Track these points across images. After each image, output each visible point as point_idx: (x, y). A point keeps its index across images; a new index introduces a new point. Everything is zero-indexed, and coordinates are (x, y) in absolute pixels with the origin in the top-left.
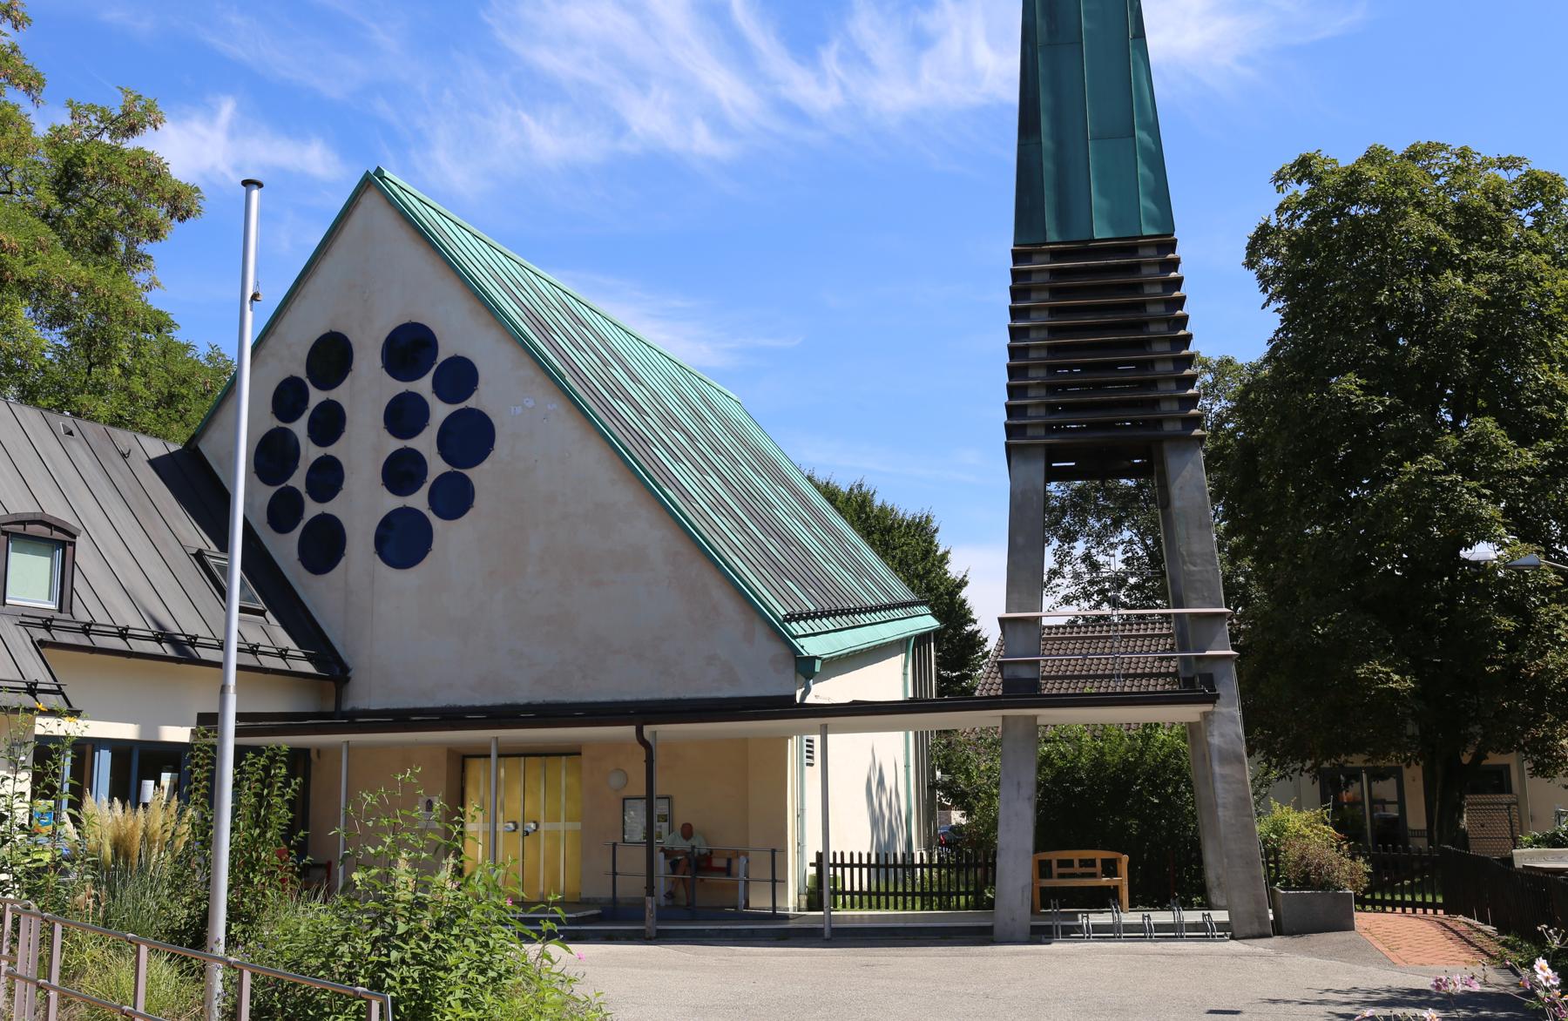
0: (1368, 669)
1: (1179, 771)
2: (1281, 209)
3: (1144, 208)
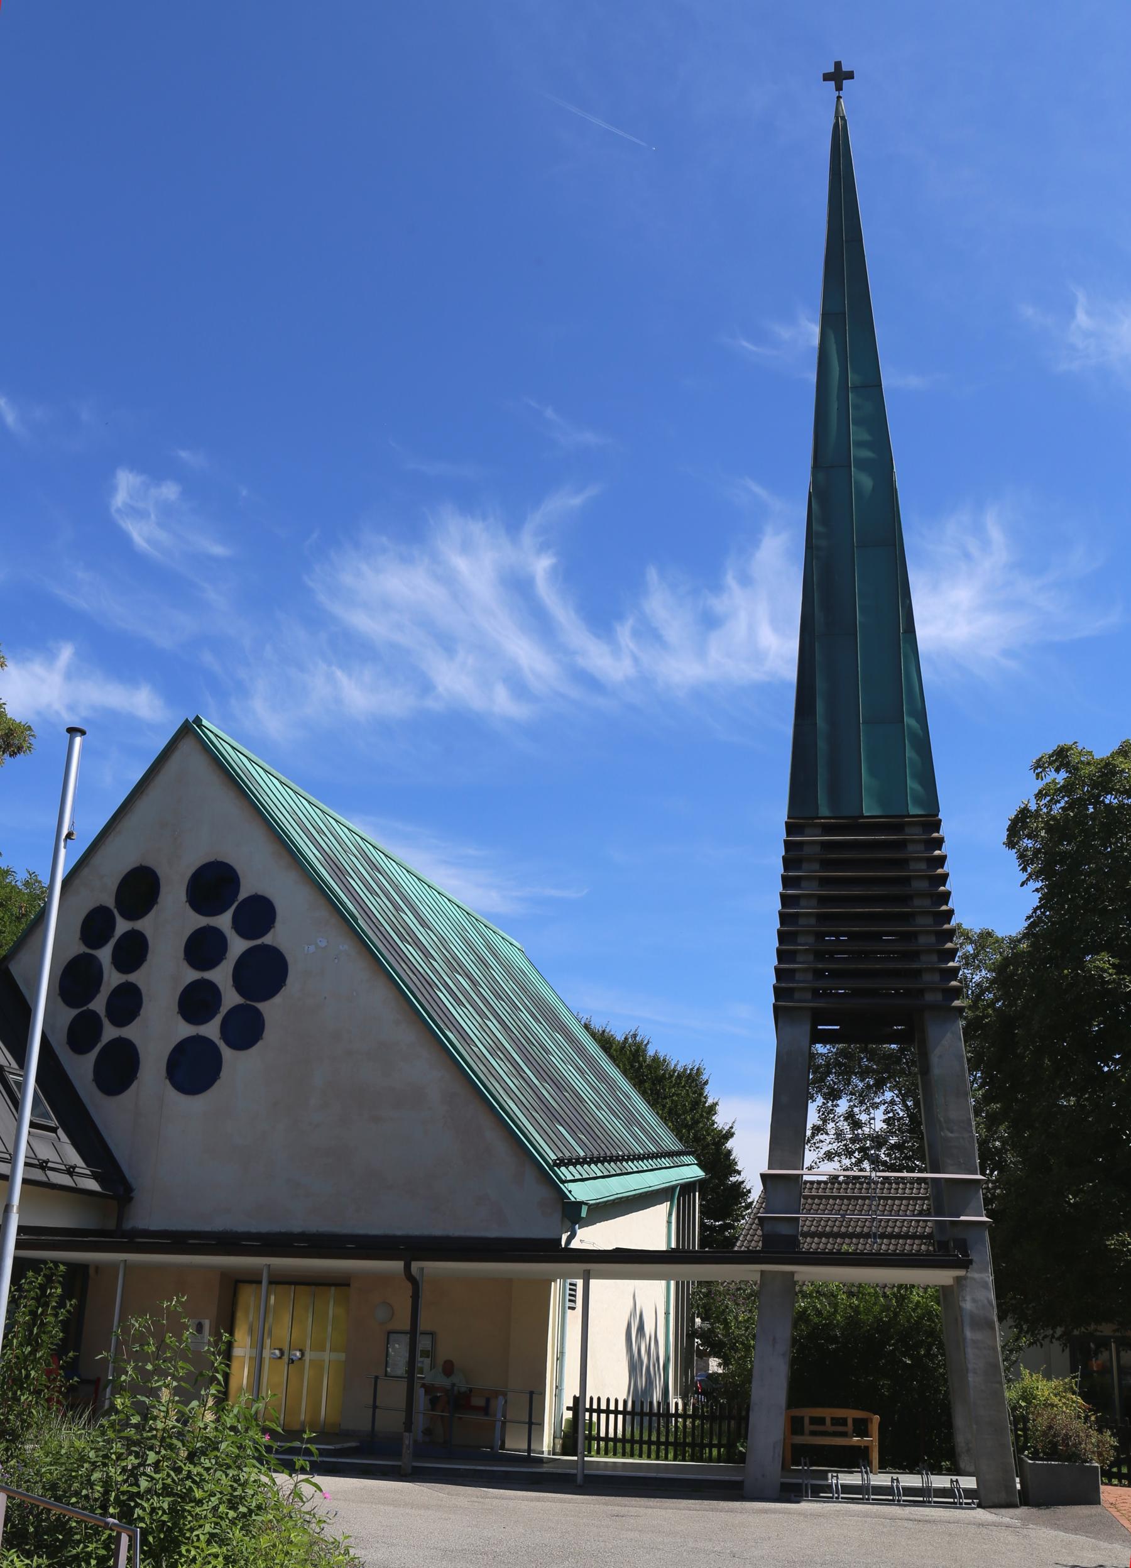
0: (1117, 1240)
1: (931, 1333)
2: (1040, 795)
3: (912, 789)
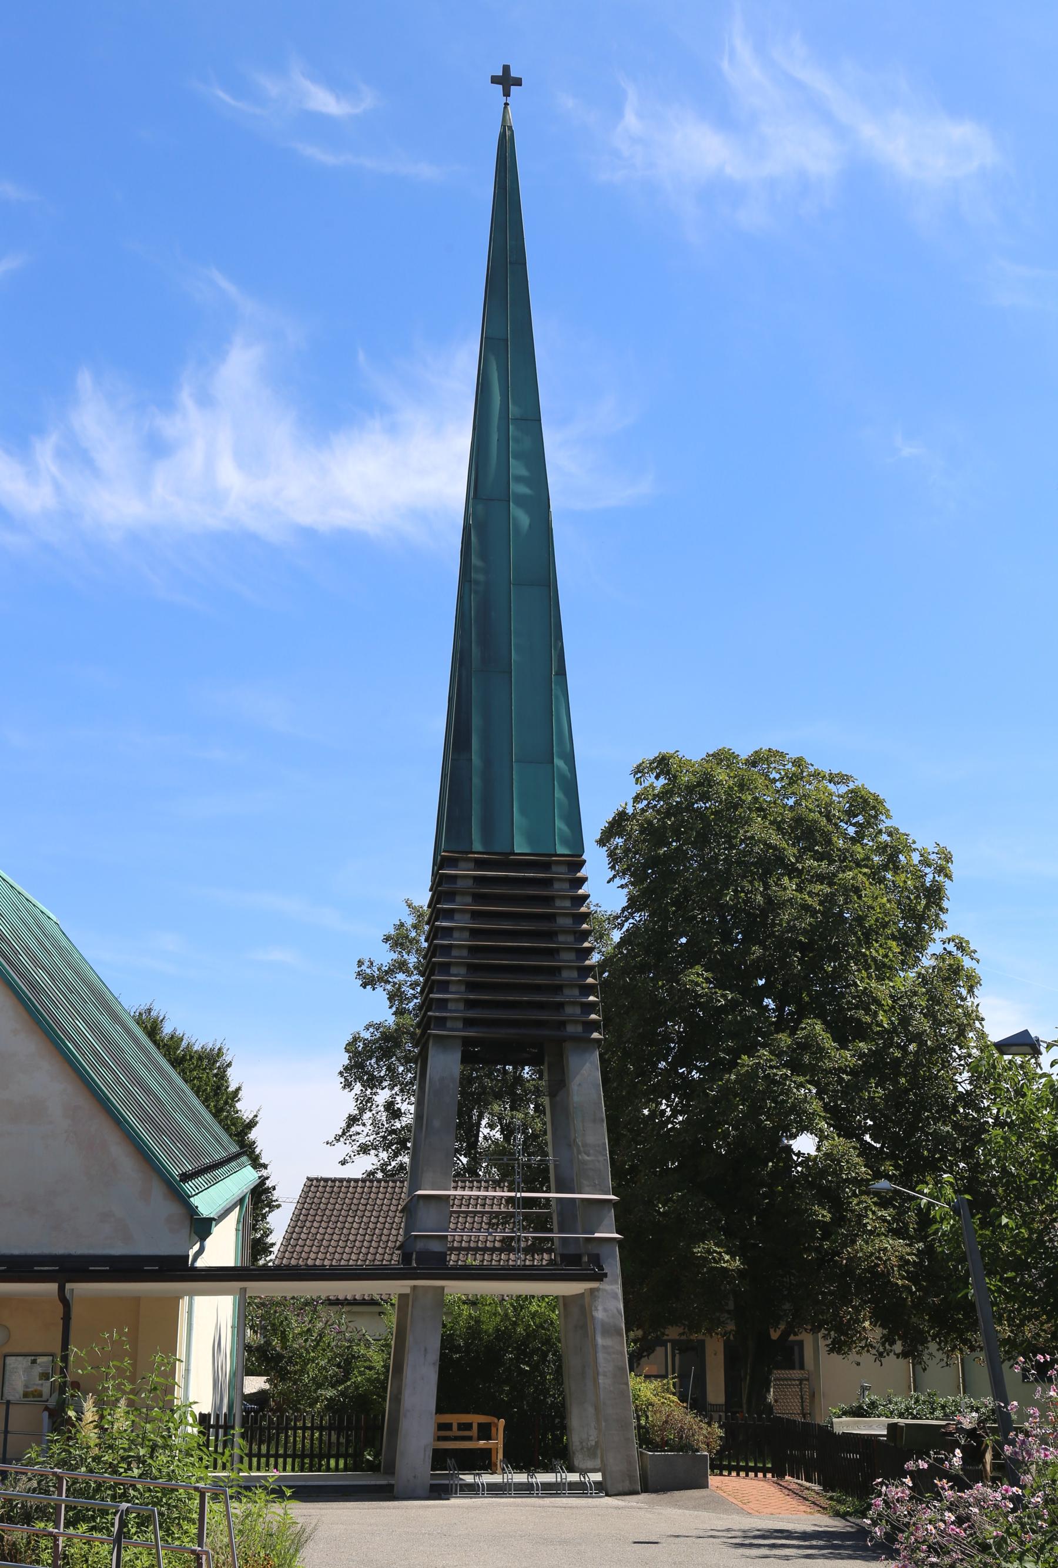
0: (704, 1248)
1: (547, 1341)
2: (637, 799)
3: (560, 829)
